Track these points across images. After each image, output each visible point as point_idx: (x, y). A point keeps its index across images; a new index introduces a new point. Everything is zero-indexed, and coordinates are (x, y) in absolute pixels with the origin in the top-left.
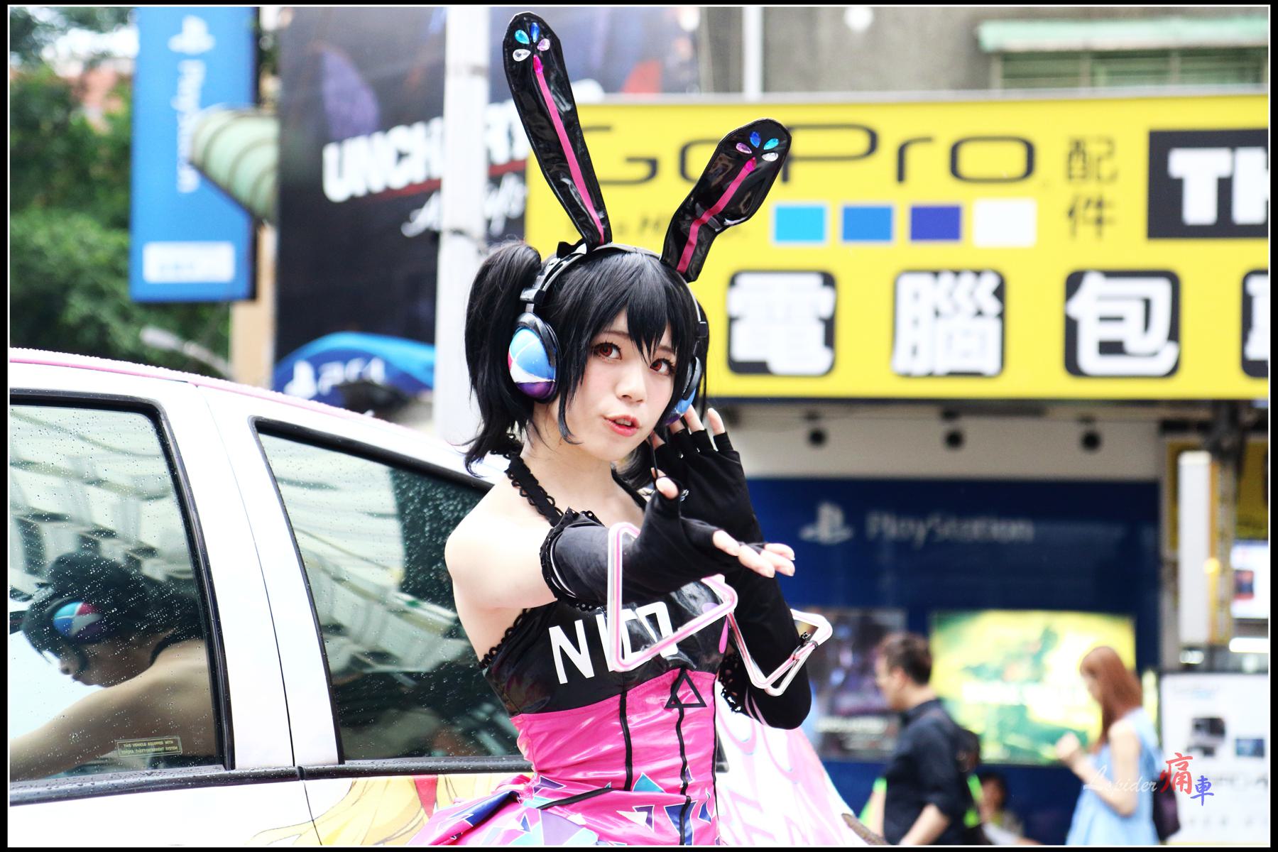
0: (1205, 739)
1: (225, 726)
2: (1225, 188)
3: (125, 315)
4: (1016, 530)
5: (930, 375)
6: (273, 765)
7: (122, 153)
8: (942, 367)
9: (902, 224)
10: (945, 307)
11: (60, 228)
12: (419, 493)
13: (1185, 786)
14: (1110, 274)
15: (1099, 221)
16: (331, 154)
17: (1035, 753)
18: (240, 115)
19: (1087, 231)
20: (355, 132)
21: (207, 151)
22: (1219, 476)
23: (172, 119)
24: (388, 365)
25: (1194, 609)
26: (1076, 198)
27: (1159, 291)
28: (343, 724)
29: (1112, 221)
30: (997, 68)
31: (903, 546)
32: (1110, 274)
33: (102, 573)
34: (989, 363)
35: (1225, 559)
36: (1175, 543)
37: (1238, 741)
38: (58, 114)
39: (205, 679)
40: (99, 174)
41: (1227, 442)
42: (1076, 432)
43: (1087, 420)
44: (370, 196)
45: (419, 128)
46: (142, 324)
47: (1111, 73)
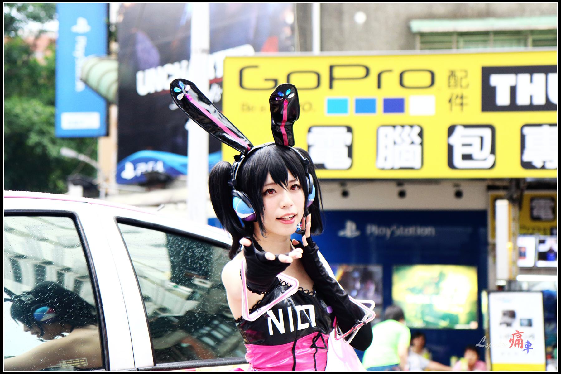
0: (508, 319)
1: (106, 352)
2: (513, 90)
3: (53, 141)
4: (428, 231)
5: (392, 169)
6: (126, 368)
7: (52, 73)
8: (397, 166)
9: (380, 106)
10: (398, 140)
11: (26, 105)
12: (185, 246)
13: (520, 345)
14: (466, 126)
15: (462, 104)
16: (140, 75)
17: (437, 324)
18: (102, 59)
19: (457, 108)
20: (150, 66)
21: (88, 75)
22: (512, 209)
23: (72, 61)
24: (165, 164)
25: (501, 268)
26: (452, 95)
27: (487, 133)
28: (153, 336)
29: (467, 104)
30: (418, 39)
31: (380, 238)
32: (466, 126)
33: (53, 289)
34: (417, 164)
35: (515, 243)
36: (494, 236)
37: (521, 320)
38: (25, 57)
39: (98, 339)
40: (44, 84)
41: (515, 196)
42: (452, 190)
43: (456, 185)
44: (156, 93)
45: (177, 65)
46: (61, 146)
47: (465, 41)
